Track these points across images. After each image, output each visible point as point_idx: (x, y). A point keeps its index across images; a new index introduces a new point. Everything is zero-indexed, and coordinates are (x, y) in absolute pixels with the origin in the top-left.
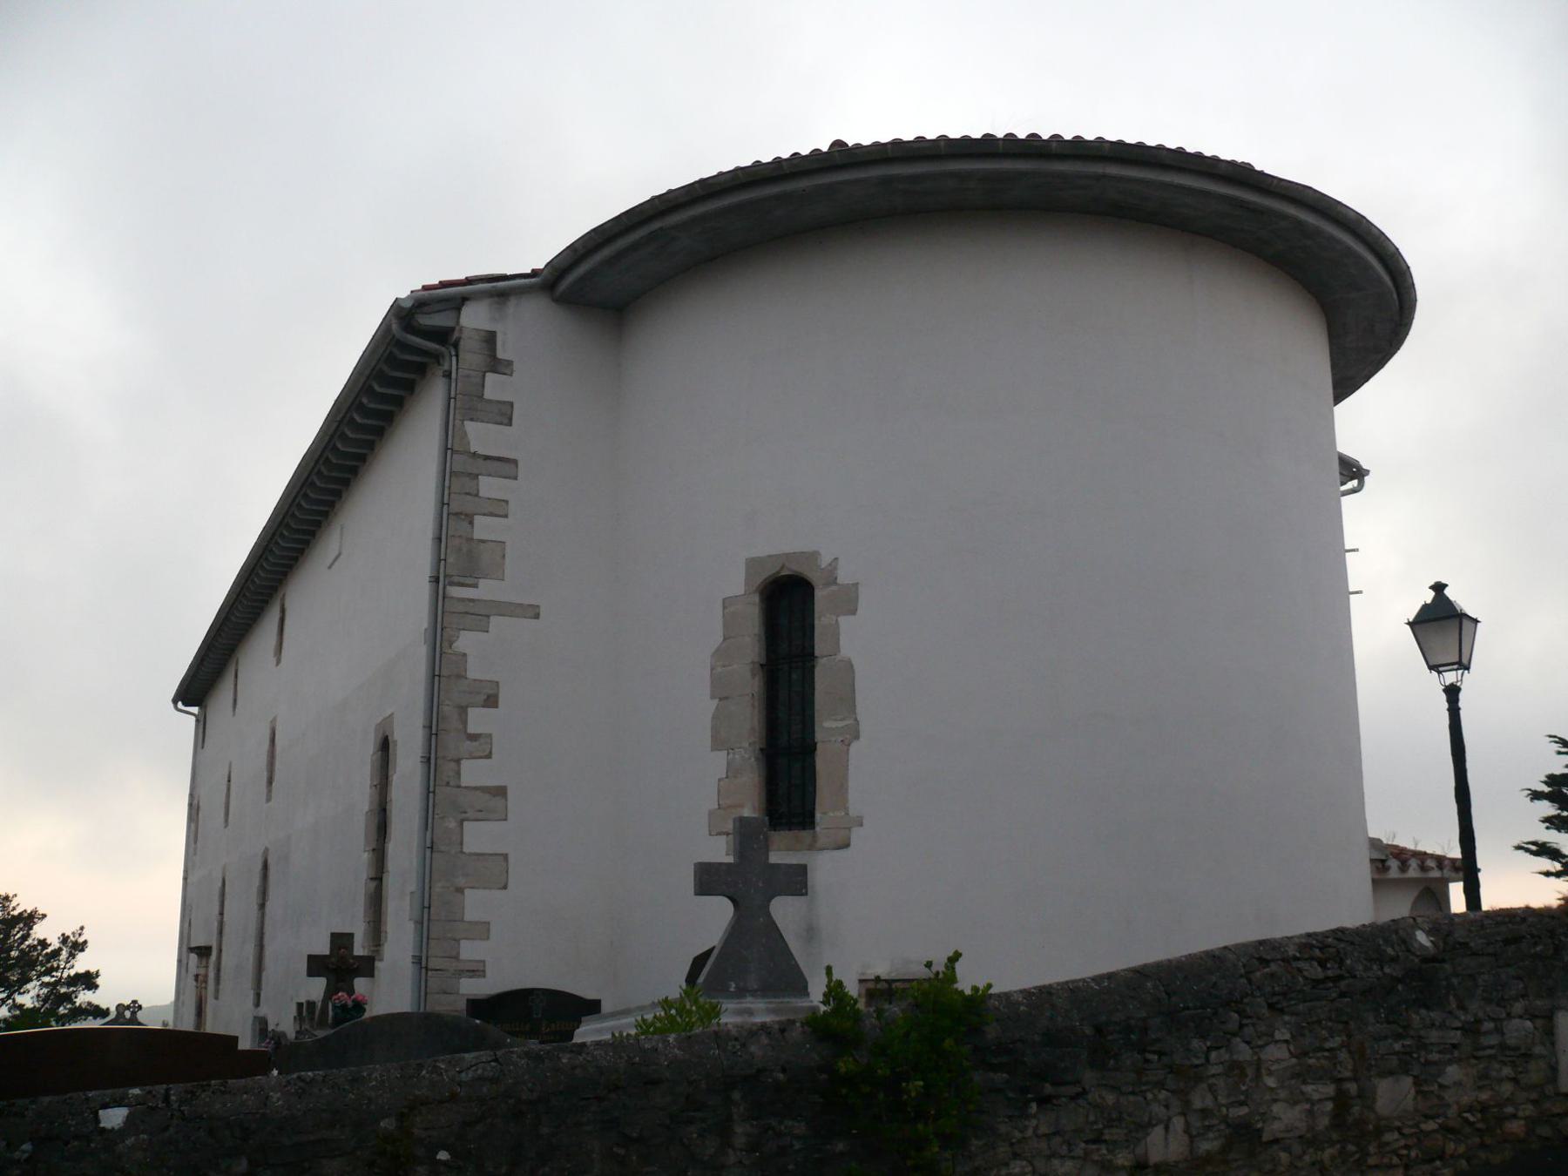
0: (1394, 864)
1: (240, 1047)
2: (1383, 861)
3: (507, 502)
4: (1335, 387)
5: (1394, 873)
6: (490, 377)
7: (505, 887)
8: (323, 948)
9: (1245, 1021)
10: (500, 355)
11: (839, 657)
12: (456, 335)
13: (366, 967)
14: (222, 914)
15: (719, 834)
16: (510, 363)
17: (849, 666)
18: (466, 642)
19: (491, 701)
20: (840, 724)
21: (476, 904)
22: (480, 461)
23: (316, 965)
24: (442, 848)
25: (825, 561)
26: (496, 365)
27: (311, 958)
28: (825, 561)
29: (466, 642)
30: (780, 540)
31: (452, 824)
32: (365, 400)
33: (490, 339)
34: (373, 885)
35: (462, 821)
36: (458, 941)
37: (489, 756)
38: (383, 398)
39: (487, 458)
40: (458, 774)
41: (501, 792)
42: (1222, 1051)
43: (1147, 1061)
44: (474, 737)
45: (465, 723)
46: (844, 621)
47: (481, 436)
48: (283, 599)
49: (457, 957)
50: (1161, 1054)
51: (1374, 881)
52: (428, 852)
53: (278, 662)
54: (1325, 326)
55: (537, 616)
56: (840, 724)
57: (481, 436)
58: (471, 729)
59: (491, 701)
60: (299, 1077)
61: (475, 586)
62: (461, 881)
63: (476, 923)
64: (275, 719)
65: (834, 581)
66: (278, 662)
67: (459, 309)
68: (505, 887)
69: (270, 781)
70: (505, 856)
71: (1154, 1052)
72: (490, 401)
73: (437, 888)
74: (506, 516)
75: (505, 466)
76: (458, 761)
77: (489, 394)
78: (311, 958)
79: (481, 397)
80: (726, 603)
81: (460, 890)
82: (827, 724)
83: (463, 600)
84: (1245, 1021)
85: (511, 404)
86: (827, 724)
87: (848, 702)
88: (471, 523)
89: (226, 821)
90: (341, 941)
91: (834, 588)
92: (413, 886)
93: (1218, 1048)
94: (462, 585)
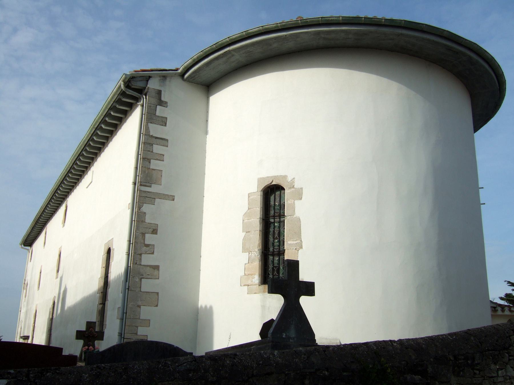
0: (499, 309)
1: (63, 354)
2: (495, 308)
3: (163, 155)
4: (474, 127)
5: (499, 312)
6: (158, 107)
7: (157, 306)
8: (84, 328)
9: (511, 358)
10: (163, 99)
11: (295, 216)
12: (146, 90)
13: (100, 336)
14: (35, 323)
15: (244, 285)
16: (166, 103)
17: (299, 220)
18: (146, 208)
19: (155, 231)
20: (295, 242)
21: (145, 312)
22: (154, 139)
23: (80, 335)
24: (133, 289)
25: (289, 179)
26: (162, 103)
27: (78, 332)
28: (289, 179)
29: (146, 208)
30: (271, 173)
31: (137, 280)
32: (107, 119)
33: (159, 93)
34: (101, 306)
35: (141, 278)
36: (137, 327)
37: (153, 253)
38: (115, 118)
39: (156, 138)
40: (141, 259)
41: (157, 268)
42: (503, 370)
43: (475, 374)
44: (147, 246)
45: (144, 240)
46: (297, 203)
47: (156, 130)
48: (67, 202)
49: (136, 334)
50: (480, 370)
51: (492, 315)
52: (127, 290)
53: (64, 226)
54: (470, 105)
55: (173, 200)
56: (295, 242)
57: (156, 130)
58: (146, 243)
59: (155, 231)
60: (97, 367)
61: (150, 187)
62: (140, 303)
63: (145, 320)
64: (61, 247)
65: (293, 187)
66: (64, 226)
67: (148, 81)
68: (157, 306)
69: (58, 271)
70: (158, 293)
71: (477, 370)
72: (158, 116)
73: (130, 305)
74: (163, 161)
75: (164, 141)
76: (141, 255)
77: (158, 113)
78: (78, 332)
79: (155, 114)
80: (249, 195)
81: (139, 306)
82: (289, 242)
83: (145, 192)
84: (511, 358)
85: (166, 118)
86: (289, 242)
87: (298, 234)
88: (150, 162)
89: (39, 287)
90: (90, 325)
91: (292, 189)
92: (119, 304)
93: (502, 369)
94: (146, 186)
